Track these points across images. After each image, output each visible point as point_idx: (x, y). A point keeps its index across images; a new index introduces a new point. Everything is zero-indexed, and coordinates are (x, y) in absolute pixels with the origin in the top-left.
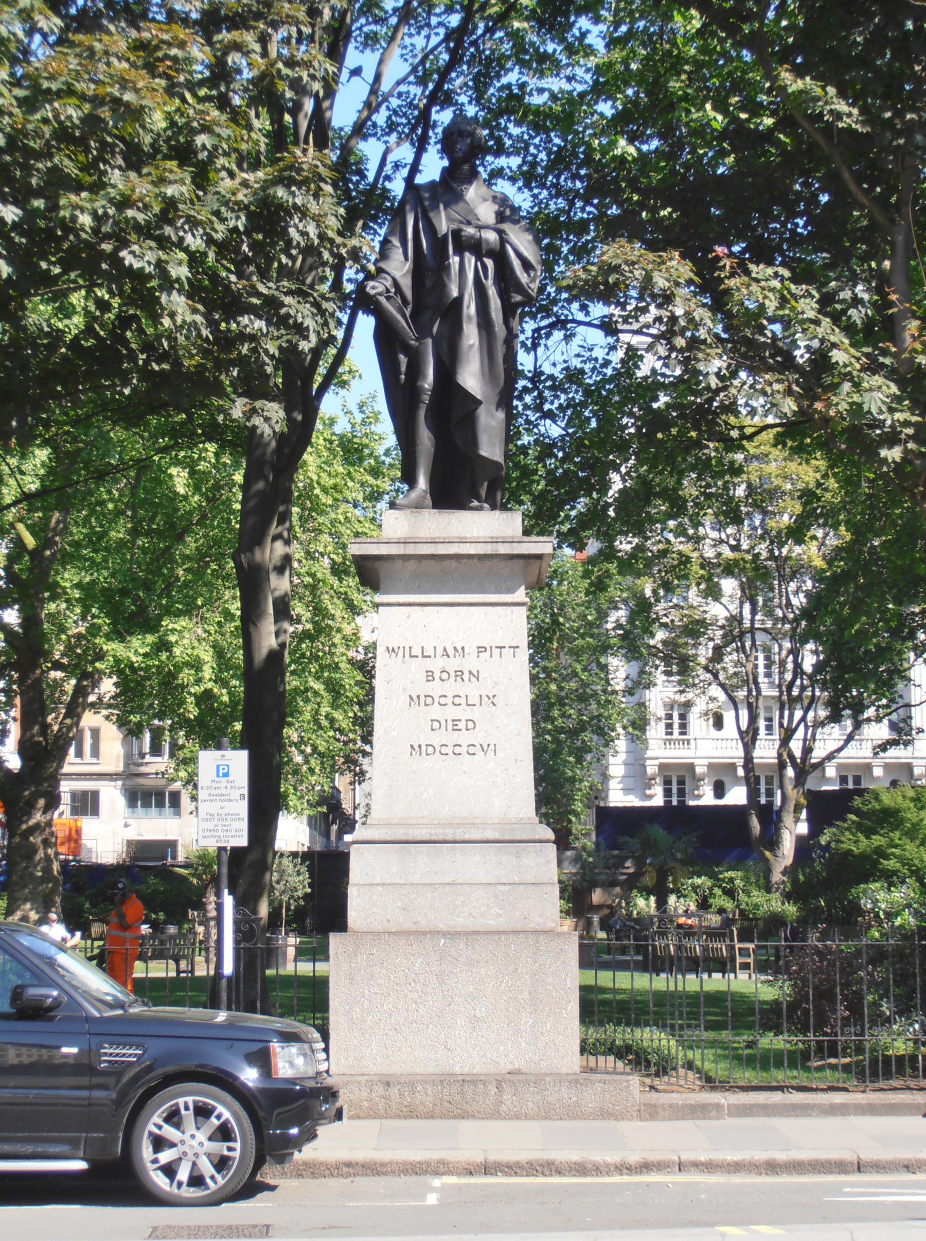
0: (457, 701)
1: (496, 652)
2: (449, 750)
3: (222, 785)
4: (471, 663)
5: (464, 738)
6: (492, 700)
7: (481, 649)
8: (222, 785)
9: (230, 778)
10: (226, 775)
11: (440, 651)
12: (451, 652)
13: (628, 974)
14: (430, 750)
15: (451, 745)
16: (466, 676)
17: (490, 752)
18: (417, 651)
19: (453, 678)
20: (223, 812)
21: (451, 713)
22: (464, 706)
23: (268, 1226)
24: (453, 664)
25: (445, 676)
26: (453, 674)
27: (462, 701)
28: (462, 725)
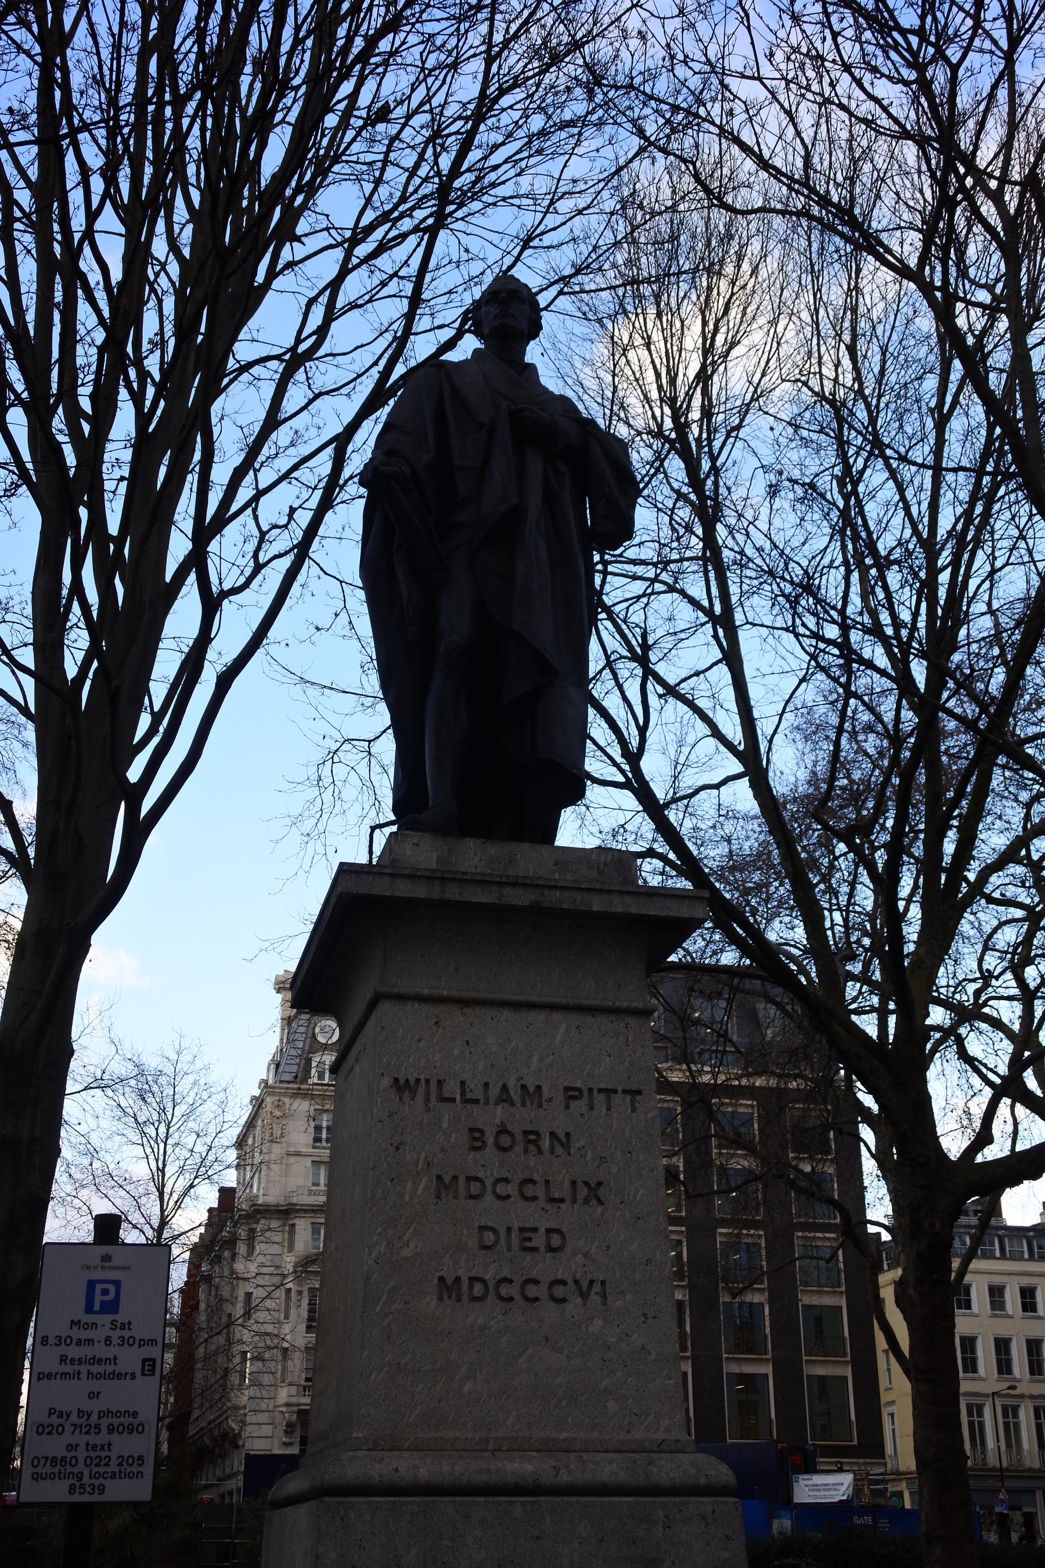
0: (529, 1190)
1: (600, 1099)
2: (513, 1290)
3: (99, 1335)
4: (555, 1118)
5: (544, 1267)
6: (594, 1192)
7: (572, 1093)
8: (99, 1335)
9: (121, 1317)
10: (111, 1307)
11: (494, 1091)
12: (515, 1093)
13: (941, 1139)
14: (478, 1289)
15: (518, 1279)
16: (546, 1143)
17: (595, 1298)
18: (452, 1088)
19: (519, 1148)
20: (95, 1406)
21: (521, 1214)
22: (542, 1202)
23: (471, 1130)
24: (521, 1118)
25: (505, 1141)
26: (519, 1137)
27: (540, 1191)
28: (538, 1240)
